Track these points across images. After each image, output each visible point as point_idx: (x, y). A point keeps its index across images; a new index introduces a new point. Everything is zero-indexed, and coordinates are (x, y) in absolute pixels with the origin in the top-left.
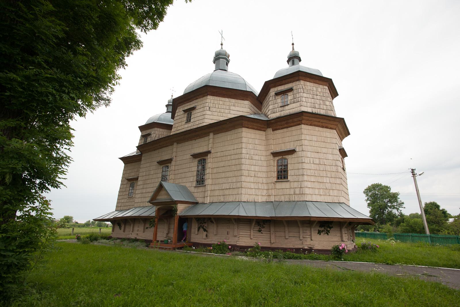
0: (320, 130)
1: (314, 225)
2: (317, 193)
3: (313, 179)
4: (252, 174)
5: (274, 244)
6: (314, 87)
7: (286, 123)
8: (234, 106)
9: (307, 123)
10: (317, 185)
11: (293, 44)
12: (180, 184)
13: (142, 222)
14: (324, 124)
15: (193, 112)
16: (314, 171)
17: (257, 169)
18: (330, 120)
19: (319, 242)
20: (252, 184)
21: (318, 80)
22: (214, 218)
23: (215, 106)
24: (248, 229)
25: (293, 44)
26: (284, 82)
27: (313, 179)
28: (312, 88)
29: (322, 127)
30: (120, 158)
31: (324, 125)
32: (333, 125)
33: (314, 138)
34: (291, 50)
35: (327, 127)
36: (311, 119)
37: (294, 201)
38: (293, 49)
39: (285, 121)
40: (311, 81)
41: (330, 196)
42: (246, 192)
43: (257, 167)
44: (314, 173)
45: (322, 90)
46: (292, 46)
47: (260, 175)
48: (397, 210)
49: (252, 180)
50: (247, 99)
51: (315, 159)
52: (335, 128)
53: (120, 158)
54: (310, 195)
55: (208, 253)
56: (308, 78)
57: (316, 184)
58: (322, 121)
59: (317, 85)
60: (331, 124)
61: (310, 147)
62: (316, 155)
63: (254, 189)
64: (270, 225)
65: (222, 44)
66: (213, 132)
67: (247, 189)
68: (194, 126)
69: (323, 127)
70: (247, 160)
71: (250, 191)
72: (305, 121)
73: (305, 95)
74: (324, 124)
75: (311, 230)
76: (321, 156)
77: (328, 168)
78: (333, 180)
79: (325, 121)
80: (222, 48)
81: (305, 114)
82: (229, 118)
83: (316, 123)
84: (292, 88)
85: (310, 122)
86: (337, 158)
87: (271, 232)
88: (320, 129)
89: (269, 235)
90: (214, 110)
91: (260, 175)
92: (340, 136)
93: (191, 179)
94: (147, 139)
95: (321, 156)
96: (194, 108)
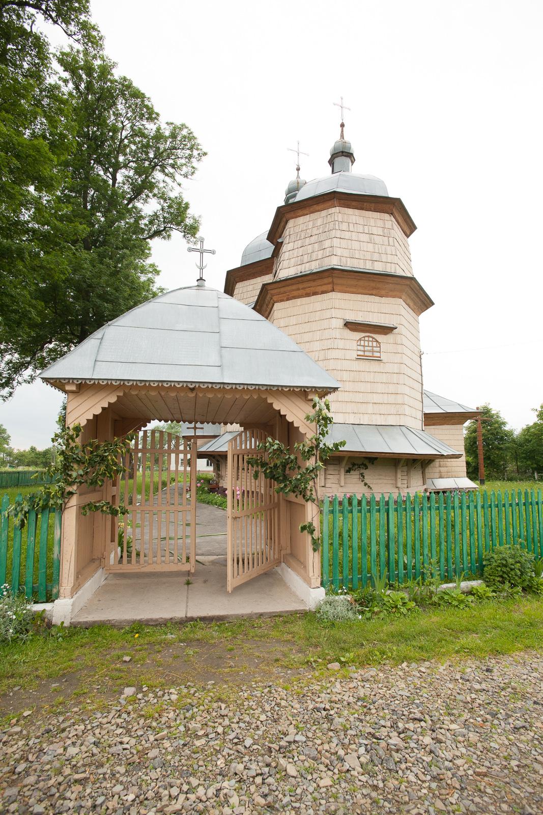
1: (401, 465)
11: (342, 125)
14: (308, 290)
18: (314, 280)
21: (315, 206)
25: (342, 125)
26: (280, 230)
29: (308, 295)
31: (309, 292)
34: (338, 138)
35: (315, 294)
36: (282, 290)
38: (342, 136)
46: (340, 129)
48: (56, 435)
55: (31, 469)
56: (300, 210)
58: (301, 286)
59: (314, 216)
60: (321, 285)
65: (298, 169)
69: (308, 295)
72: (278, 296)
74: (308, 290)
75: (396, 473)
79: (305, 285)
80: (298, 177)
81: (269, 287)
83: (295, 293)
85: (284, 295)
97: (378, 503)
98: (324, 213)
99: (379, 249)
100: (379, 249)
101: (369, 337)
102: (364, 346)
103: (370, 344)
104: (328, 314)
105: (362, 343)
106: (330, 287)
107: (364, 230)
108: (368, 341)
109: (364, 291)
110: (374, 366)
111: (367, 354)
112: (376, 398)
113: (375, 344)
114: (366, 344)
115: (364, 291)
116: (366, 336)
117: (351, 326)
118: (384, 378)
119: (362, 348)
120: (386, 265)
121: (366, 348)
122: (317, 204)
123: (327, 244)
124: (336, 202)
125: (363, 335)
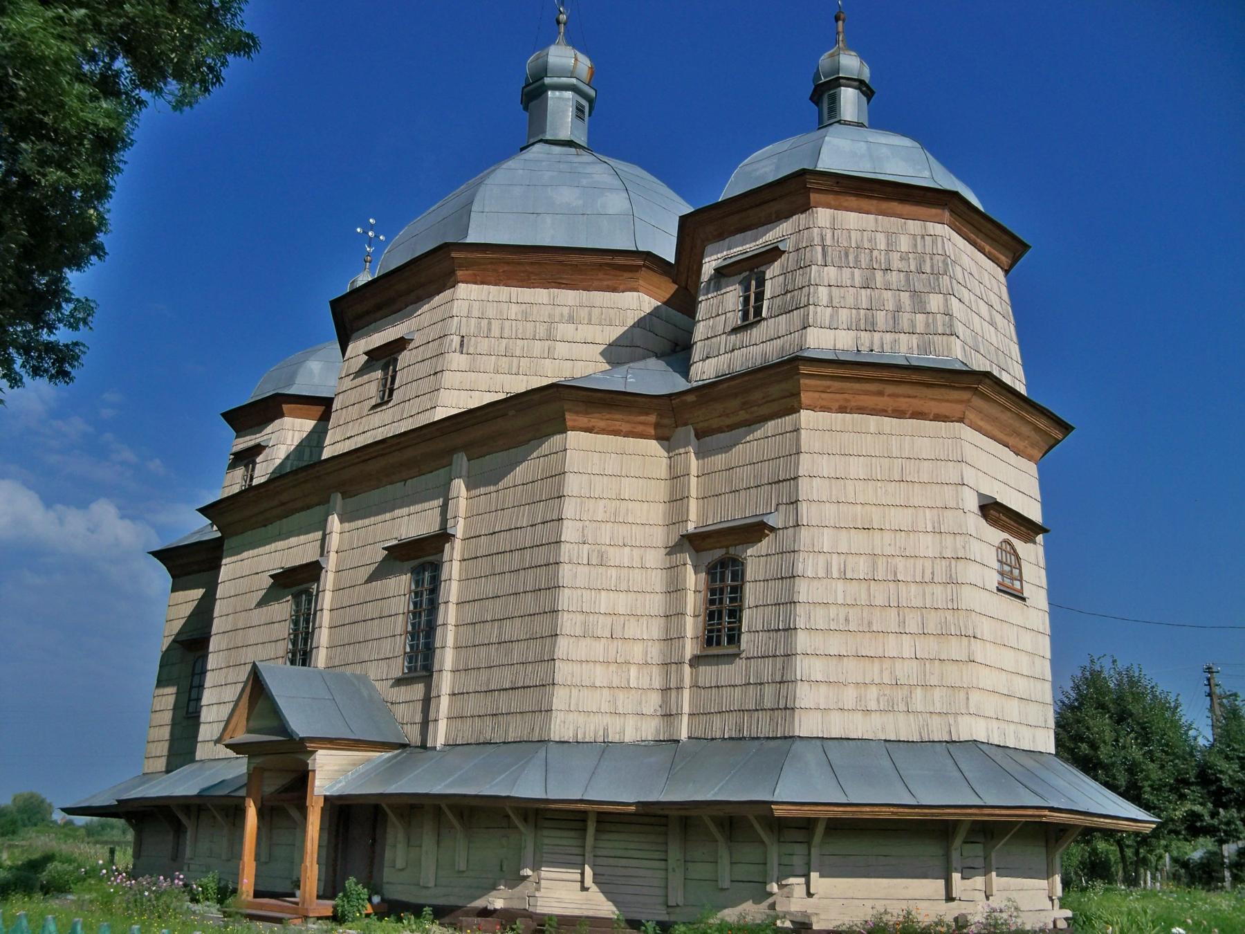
0: (887, 430)
2: (849, 704)
3: (835, 645)
4: (602, 626)
5: (678, 910)
6: (878, 235)
7: (745, 406)
8: (571, 320)
9: (824, 403)
10: (852, 670)
12: (348, 671)
13: (455, 822)
15: (404, 358)
16: (842, 612)
17: (622, 603)
19: (845, 902)
20: (599, 669)
22: (517, 810)
23: (489, 330)
24: (656, 855)
27: (835, 645)
28: (870, 241)
30: (156, 554)
31: (904, 407)
32: (947, 401)
33: (857, 467)
37: (753, 738)
39: (736, 395)
40: (864, 203)
41: (911, 716)
42: (573, 702)
43: (623, 596)
44: (842, 620)
45: (915, 245)
47: (633, 629)
49: (599, 649)
50: (633, 284)
51: (851, 561)
52: (959, 415)
53: (156, 554)
54: (819, 714)
57: (850, 664)
61: (834, 507)
62: (860, 541)
63: (606, 691)
64: (666, 834)
66: (466, 447)
67: (575, 691)
68: (401, 423)
69: (899, 414)
70: (580, 567)
71: (590, 700)
72: (817, 395)
73: (831, 273)
74: (903, 403)
76: (883, 543)
77: (912, 594)
78: (929, 647)
82: (502, 396)
84: (777, 247)
86: (958, 546)
87: (670, 861)
88: (888, 423)
89: (661, 874)
90: (484, 345)
91: (633, 629)
92: (1011, 441)
93: (387, 647)
94: (253, 470)
95: (883, 543)
96: (400, 344)
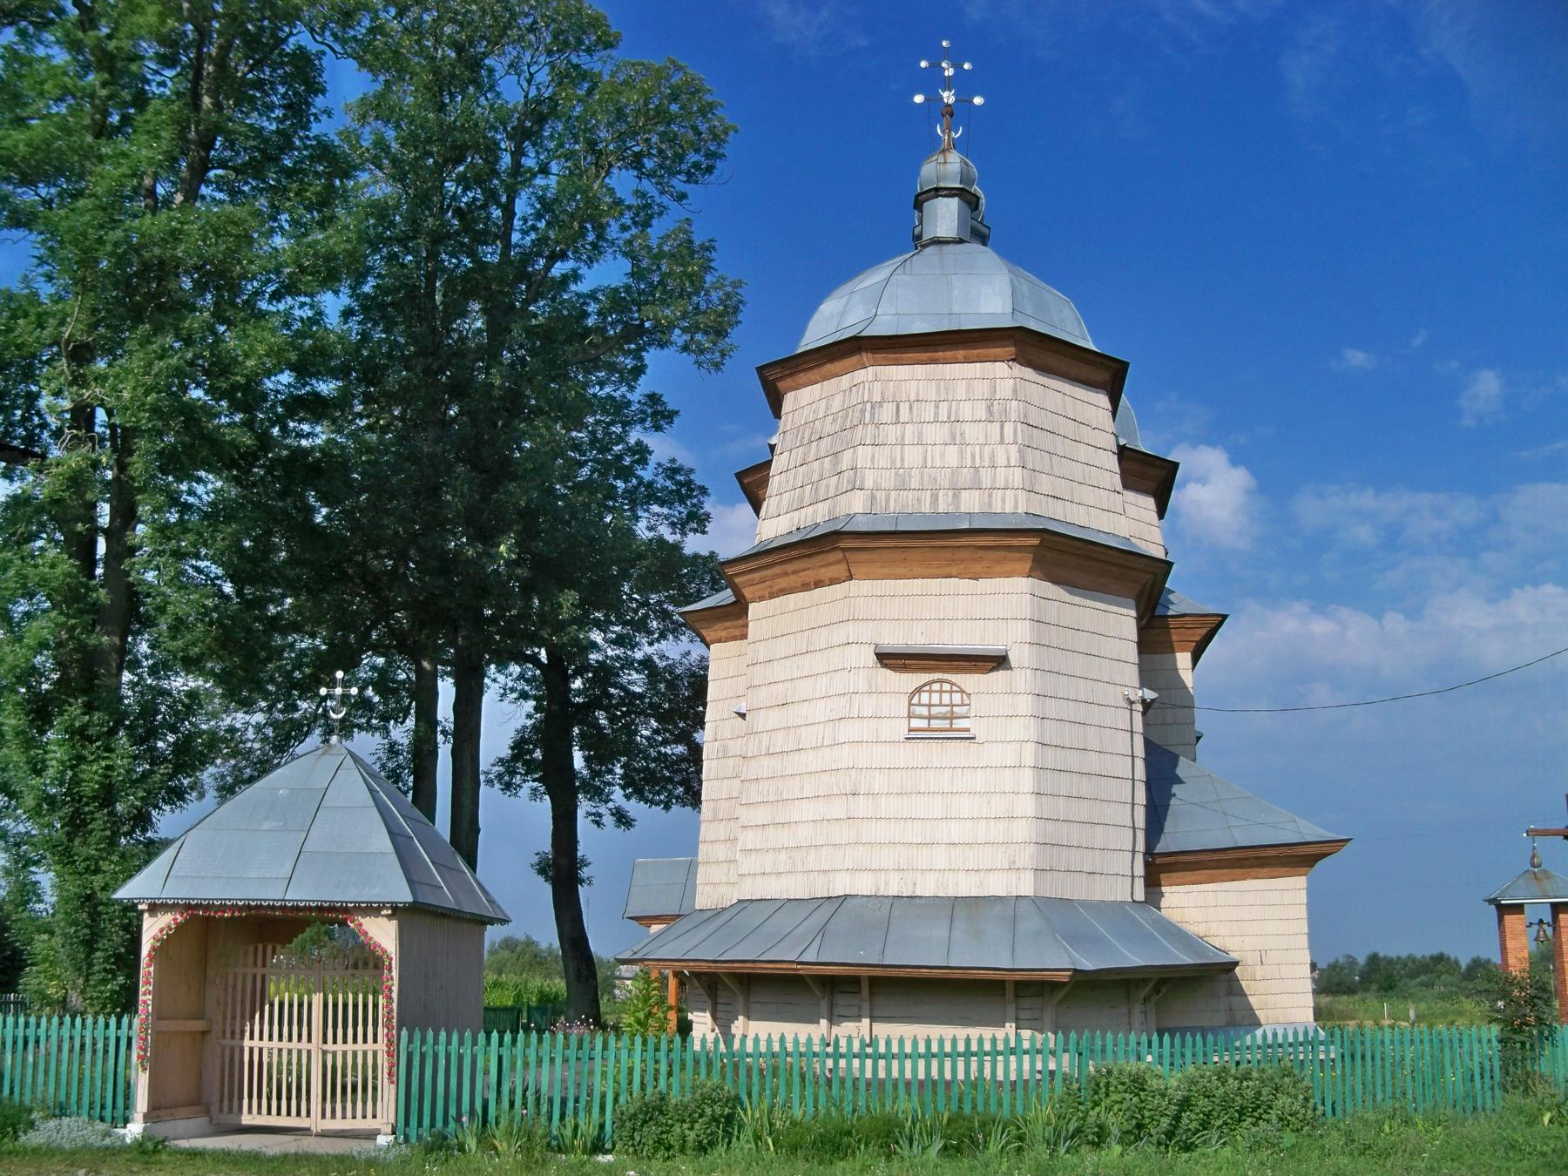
35: (818, 584)
69: (806, 587)
97: (842, 1081)
98: (845, 381)
99: (973, 458)
100: (973, 458)
101: (941, 681)
102: (930, 705)
103: (946, 697)
104: (840, 634)
105: (925, 698)
106: (840, 570)
107: (936, 414)
108: (941, 692)
109: (939, 571)
110: (953, 753)
111: (935, 724)
112: (957, 832)
113: (957, 698)
114: (935, 698)
115: (939, 571)
116: (933, 682)
117: (889, 659)
118: (979, 781)
119: (924, 711)
120: (990, 496)
121: (934, 710)
122: (832, 360)
123: (846, 460)
124: (866, 357)
125: (925, 677)
